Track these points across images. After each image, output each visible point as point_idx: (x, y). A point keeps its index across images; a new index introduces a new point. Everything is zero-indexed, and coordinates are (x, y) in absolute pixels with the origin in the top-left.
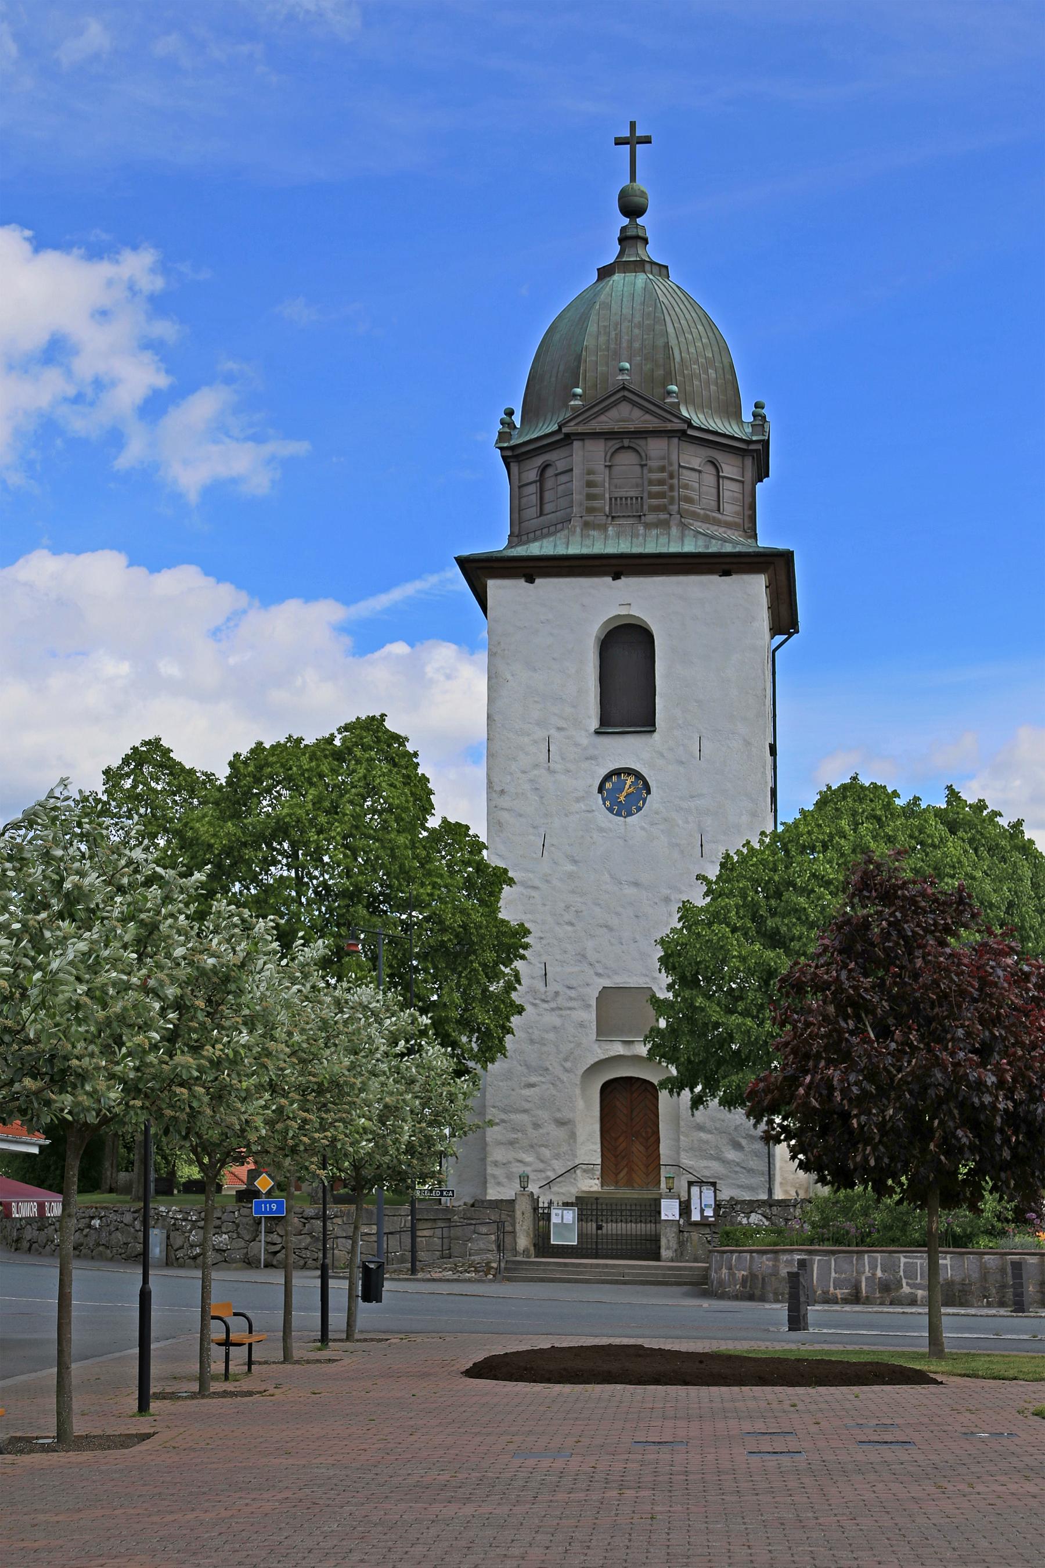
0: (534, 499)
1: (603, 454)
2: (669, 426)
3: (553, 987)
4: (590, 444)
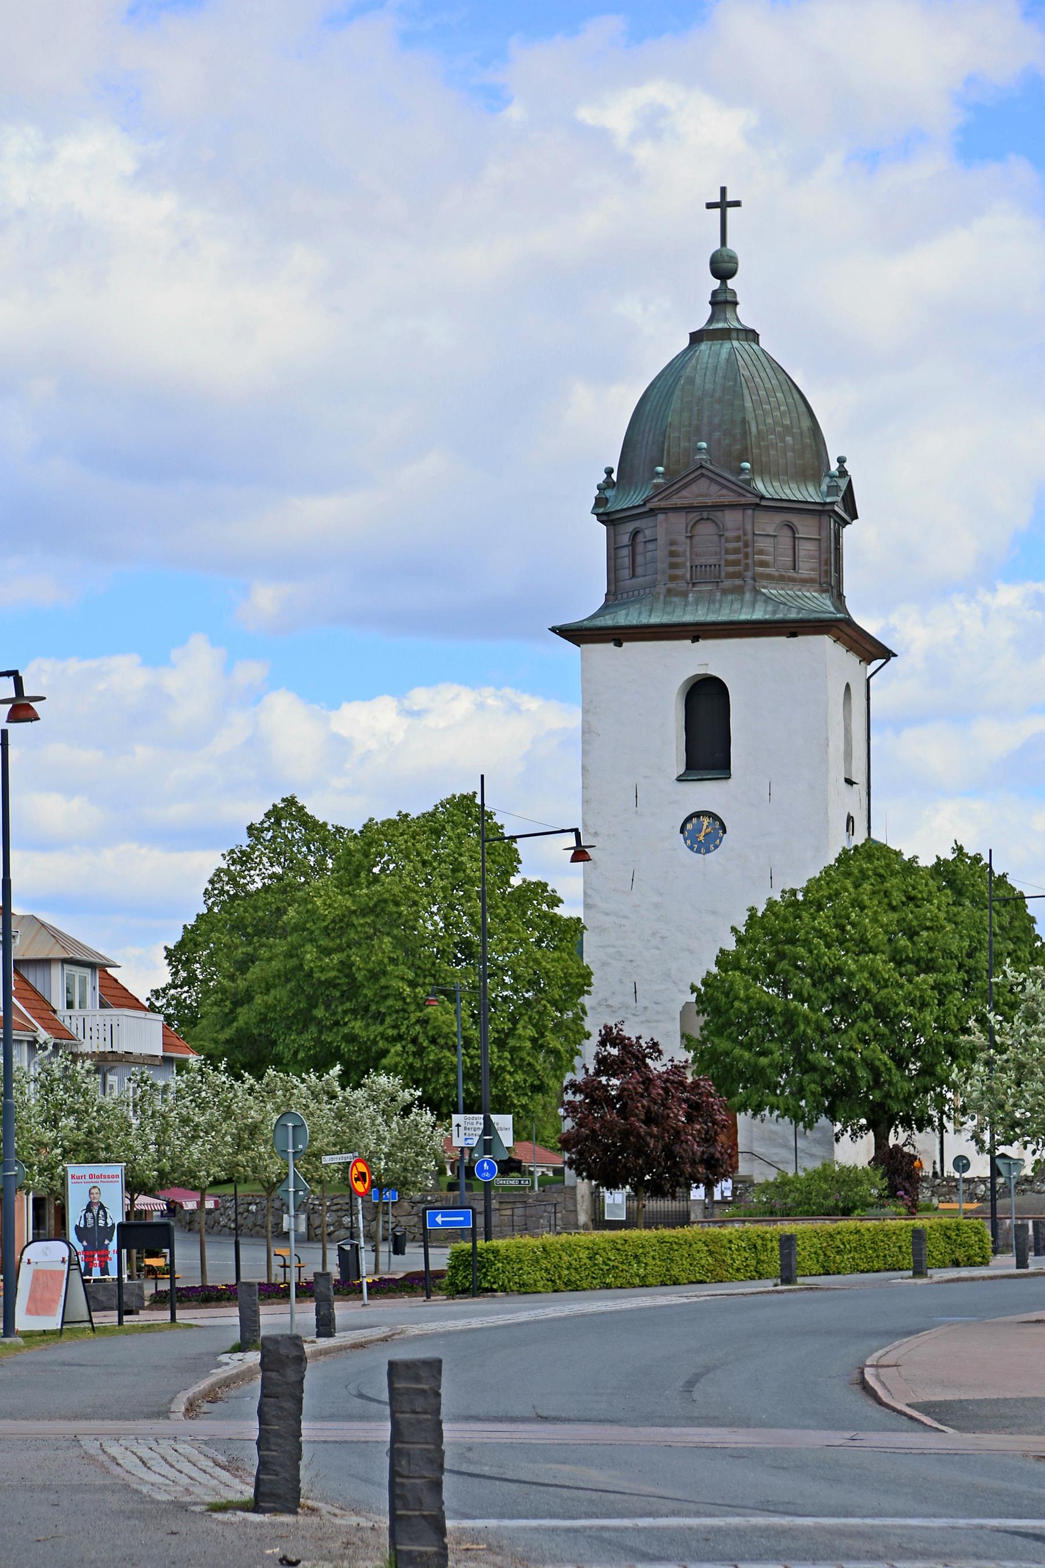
0: (627, 562)
1: (684, 526)
2: (743, 500)
3: (642, 1002)
4: (673, 517)
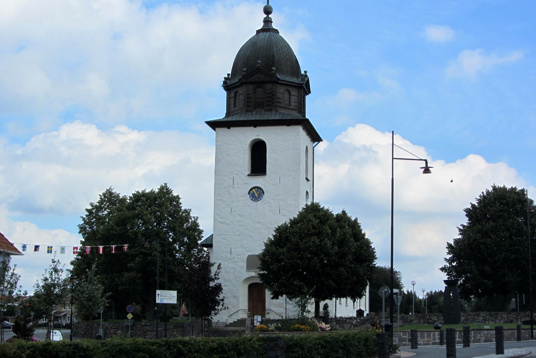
0: (233, 102)
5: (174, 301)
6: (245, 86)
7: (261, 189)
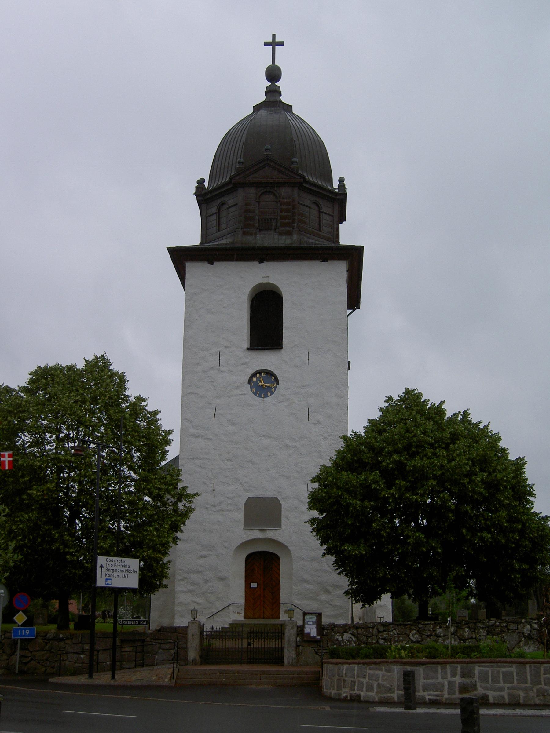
0: (215, 223)
5: (256, 586)
6: (240, 190)
7: (272, 374)
